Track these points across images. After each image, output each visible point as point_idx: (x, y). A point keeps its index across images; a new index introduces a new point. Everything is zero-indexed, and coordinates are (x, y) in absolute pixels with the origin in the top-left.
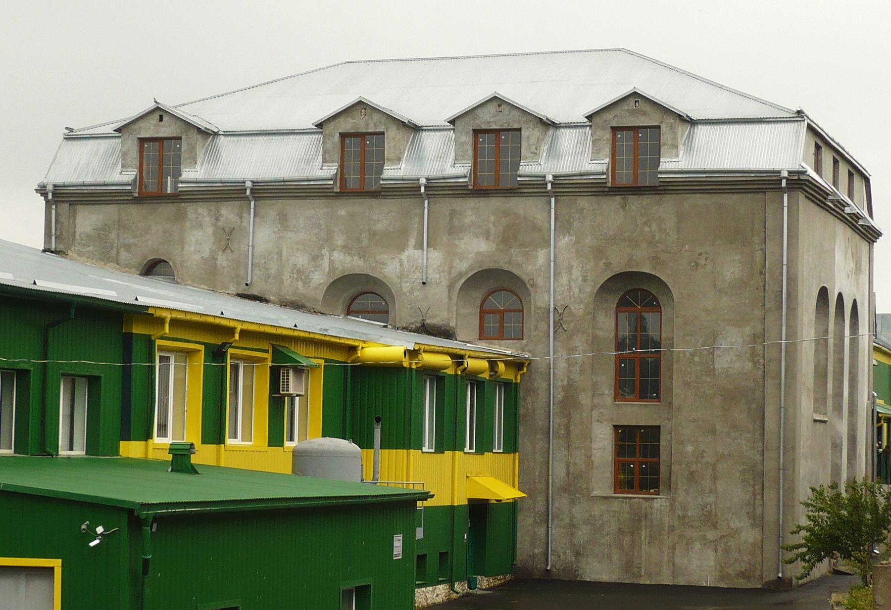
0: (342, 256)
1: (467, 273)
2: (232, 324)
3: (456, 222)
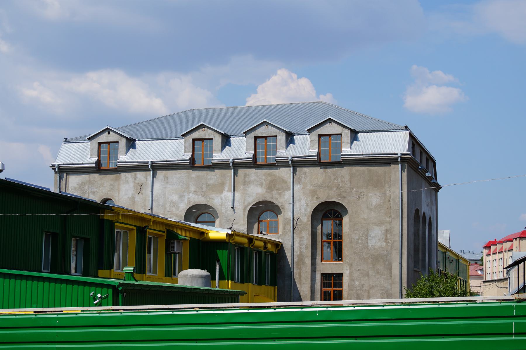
1: (252, 203)
2: (149, 217)
3: (247, 179)
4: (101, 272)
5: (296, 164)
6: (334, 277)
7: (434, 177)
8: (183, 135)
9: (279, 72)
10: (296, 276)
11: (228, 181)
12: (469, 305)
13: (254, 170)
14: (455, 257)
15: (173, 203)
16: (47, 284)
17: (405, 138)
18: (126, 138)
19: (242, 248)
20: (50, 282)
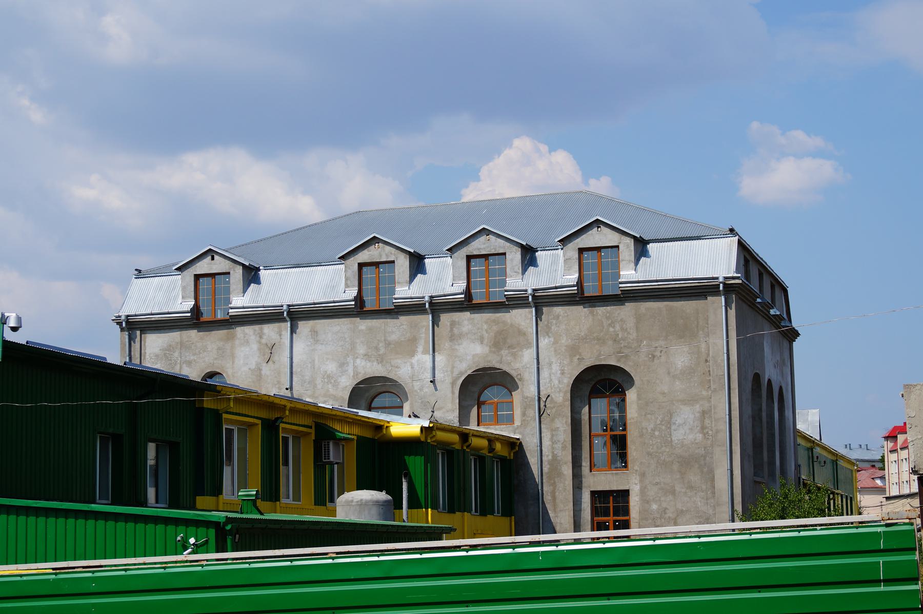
0: (363, 363)
1: (466, 371)
2: (283, 403)
3: (456, 331)
4: (200, 501)
5: (541, 301)
6: (614, 497)
7: (785, 316)
8: (343, 258)
9: (517, 142)
10: (547, 498)
11: (423, 335)
12: (802, 534)
13: (468, 314)
14: (830, 457)
15: (329, 376)
16: (101, 523)
17: (731, 250)
18: (243, 265)
19: (449, 451)
20: (96, 519)
